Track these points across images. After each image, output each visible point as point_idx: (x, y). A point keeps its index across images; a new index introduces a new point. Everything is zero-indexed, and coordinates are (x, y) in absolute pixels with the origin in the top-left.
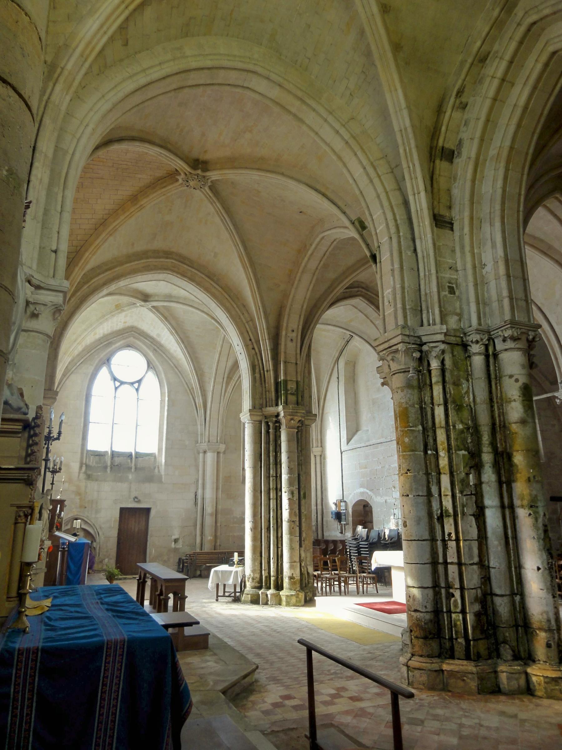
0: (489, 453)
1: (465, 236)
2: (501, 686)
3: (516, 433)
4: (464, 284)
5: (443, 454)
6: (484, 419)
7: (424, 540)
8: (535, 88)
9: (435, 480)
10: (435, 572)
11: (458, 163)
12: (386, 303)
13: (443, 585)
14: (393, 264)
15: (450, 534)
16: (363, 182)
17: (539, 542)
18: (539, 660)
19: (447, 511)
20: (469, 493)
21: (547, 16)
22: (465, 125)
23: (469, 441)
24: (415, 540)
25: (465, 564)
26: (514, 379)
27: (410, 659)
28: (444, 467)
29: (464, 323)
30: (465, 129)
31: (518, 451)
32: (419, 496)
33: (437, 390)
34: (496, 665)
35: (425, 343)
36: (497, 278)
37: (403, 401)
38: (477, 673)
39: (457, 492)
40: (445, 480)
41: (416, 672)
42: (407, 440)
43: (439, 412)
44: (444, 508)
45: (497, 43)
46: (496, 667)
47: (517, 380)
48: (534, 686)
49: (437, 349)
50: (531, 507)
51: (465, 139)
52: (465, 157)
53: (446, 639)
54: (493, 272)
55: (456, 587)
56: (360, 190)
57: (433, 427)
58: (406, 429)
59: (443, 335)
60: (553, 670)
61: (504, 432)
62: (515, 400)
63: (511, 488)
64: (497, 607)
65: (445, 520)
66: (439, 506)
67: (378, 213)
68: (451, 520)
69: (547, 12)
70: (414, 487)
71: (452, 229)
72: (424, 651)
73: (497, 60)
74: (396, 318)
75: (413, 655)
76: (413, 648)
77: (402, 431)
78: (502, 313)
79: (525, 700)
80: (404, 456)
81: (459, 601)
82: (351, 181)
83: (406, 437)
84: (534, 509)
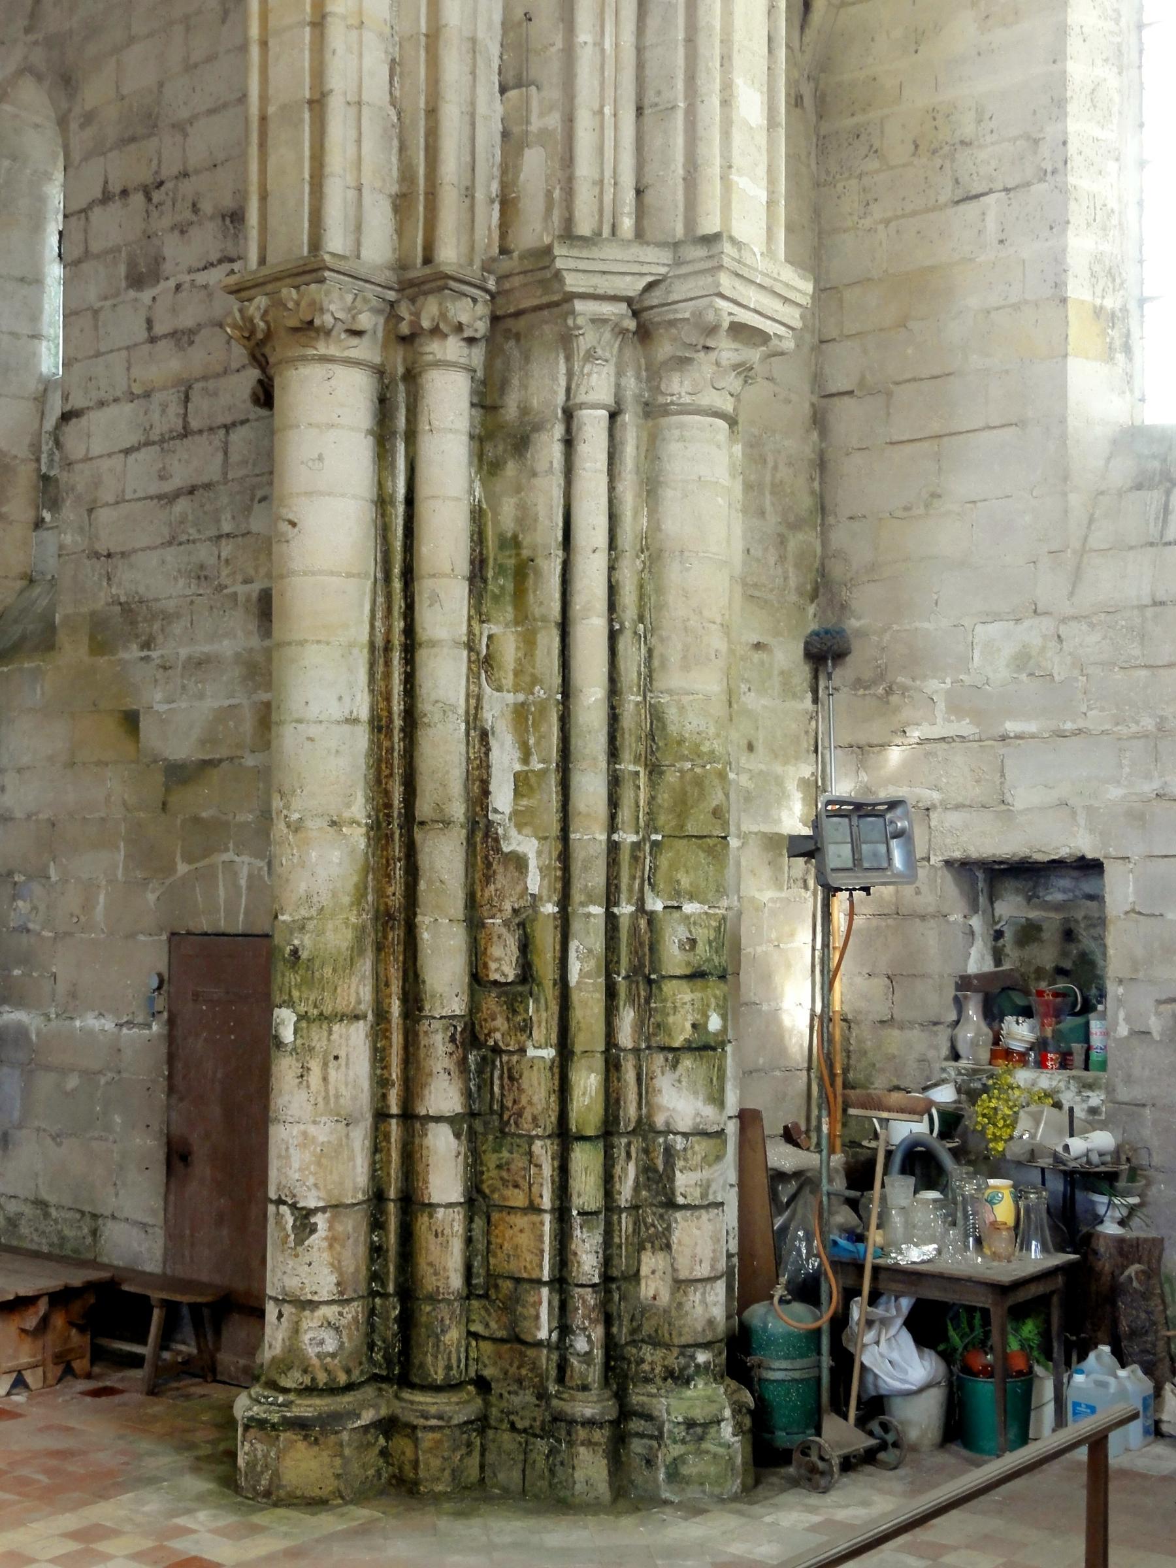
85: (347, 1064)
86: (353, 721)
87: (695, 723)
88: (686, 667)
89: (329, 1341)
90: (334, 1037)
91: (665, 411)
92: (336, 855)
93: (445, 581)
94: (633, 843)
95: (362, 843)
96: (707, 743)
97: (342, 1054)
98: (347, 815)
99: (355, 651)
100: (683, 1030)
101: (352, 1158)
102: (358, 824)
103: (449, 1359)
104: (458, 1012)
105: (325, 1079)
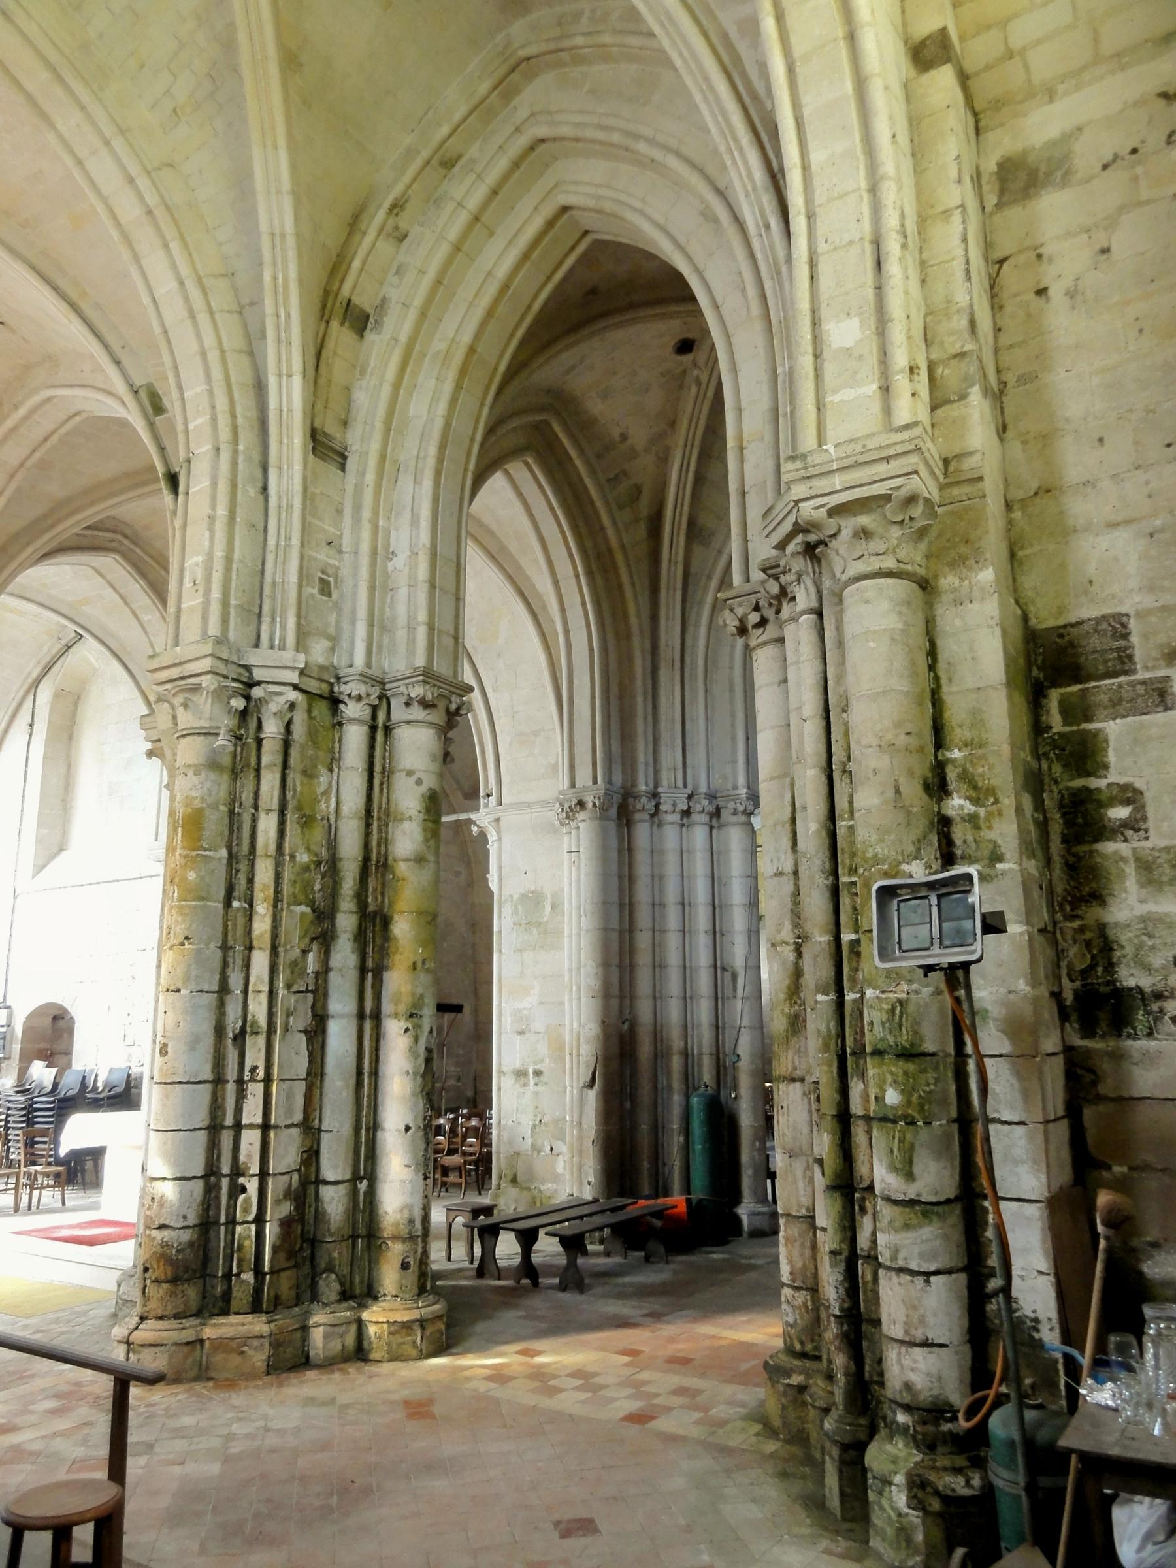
5: (262, 909)
7: (200, 1082)
8: (526, 256)
9: (239, 962)
10: (213, 1146)
11: (373, 342)
12: (188, 584)
13: (226, 1170)
15: (254, 1069)
16: (174, 311)
17: (415, 1079)
18: (385, 1295)
24: (180, 1082)
25: (276, 1127)
26: (415, 777)
27: (136, 1328)
29: (339, 656)
31: (402, 912)
32: (202, 991)
33: (270, 782)
34: (307, 1314)
35: (259, 683)
37: (194, 794)
38: (270, 1335)
39: (281, 985)
40: (260, 961)
41: (146, 1350)
42: (192, 876)
43: (267, 825)
44: (249, 1017)
46: (307, 1319)
47: (419, 782)
48: (371, 1343)
49: (281, 700)
50: (411, 1016)
51: (393, 301)
56: (163, 325)
59: (297, 673)
61: (383, 876)
64: (326, 1206)
65: (249, 1041)
66: (240, 1012)
68: (261, 1041)
69: (566, 131)
71: (343, 468)
72: (169, 1307)
74: (205, 618)
75: (143, 1319)
77: (186, 856)
78: (411, 652)
80: (180, 908)
82: (146, 300)
84: (415, 1020)
97: (785, 1106)
98: (778, 939)
99: (779, 828)
101: (795, 1182)
102: (787, 944)
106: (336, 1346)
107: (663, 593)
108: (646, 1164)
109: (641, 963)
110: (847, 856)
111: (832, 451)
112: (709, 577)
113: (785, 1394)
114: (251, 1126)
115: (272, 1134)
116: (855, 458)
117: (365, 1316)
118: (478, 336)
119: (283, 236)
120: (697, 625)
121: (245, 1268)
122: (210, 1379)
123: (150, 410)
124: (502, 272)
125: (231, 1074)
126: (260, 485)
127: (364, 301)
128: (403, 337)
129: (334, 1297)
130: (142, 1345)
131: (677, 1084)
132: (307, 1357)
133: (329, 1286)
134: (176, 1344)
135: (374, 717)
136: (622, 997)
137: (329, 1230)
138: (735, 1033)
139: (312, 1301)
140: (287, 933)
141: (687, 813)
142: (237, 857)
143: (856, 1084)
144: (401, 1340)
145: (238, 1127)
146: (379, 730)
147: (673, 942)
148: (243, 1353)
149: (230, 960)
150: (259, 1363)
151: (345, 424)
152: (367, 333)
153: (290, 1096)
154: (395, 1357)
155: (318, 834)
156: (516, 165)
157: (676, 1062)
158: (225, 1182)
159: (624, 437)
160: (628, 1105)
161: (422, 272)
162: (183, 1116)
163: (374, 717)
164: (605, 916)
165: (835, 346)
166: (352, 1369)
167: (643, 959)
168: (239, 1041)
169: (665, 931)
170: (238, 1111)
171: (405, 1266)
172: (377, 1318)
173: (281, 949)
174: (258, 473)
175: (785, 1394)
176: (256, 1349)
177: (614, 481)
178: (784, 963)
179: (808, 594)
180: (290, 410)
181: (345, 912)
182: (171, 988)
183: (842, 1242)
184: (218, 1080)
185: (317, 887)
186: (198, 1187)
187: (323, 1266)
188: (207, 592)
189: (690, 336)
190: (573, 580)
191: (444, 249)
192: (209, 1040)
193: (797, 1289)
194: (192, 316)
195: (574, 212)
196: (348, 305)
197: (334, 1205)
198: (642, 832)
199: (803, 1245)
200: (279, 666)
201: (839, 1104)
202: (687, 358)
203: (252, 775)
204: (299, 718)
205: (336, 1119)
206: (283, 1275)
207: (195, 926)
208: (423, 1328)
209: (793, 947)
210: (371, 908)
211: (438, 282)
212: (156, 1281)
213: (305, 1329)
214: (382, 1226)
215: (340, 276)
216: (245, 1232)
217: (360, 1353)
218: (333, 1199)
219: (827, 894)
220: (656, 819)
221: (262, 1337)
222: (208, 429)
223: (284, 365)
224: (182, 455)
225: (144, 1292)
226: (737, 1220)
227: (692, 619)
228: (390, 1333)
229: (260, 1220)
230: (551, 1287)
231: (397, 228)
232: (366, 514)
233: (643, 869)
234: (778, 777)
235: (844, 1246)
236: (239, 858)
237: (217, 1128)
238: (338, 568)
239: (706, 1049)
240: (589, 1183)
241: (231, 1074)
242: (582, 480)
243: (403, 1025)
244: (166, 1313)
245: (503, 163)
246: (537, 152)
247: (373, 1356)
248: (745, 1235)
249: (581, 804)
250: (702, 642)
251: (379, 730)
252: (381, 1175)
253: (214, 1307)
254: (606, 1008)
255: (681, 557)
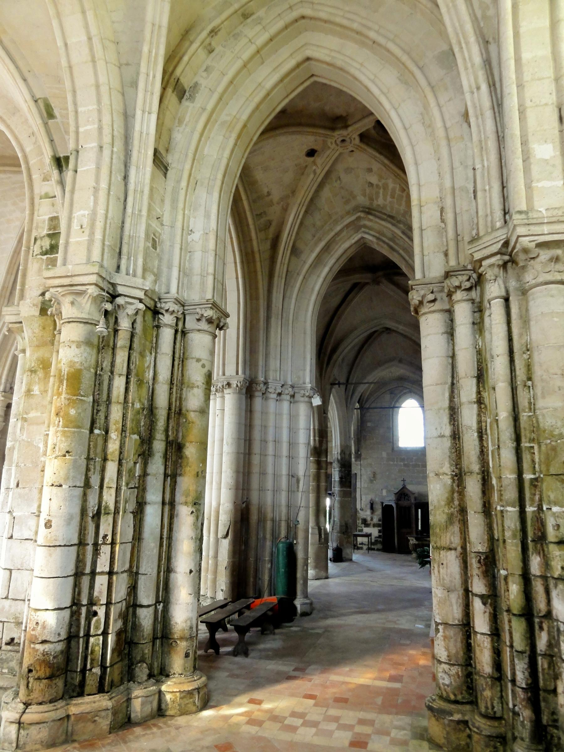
0: (162, 440)
1: (181, 191)
2: (133, 716)
3: (193, 423)
4: (168, 243)
5: (114, 435)
6: (162, 400)
7: (72, 545)
8: (281, 80)
9: (98, 468)
10: (77, 585)
11: (188, 107)
12: (75, 226)
13: (85, 602)
14: (97, 181)
15: (105, 536)
16: (79, 55)
17: (196, 542)
18: (174, 674)
19: (107, 507)
20: (133, 486)
21: (320, 19)
22: (206, 70)
23: (142, 424)
24: (60, 546)
25: (117, 573)
26: (201, 363)
27: (24, 712)
28: (113, 452)
29: (160, 286)
30: (204, 74)
31: (191, 442)
32: (75, 486)
33: (121, 357)
34: (128, 691)
35: (120, 295)
36: (205, 251)
37: (76, 360)
38: (112, 708)
39: (124, 484)
40: (112, 468)
41: (33, 727)
42: (73, 412)
43: (119, 383)
44: (104, 503)
45: (264, 9)
46: (129, 694)
47: (203, 366)
48: (167, 705)
49: (133, 307)
50: (195, 504)
51: (203, 86)
52: (199, 105)
53: (77, 672)
54: (201, 242)
55: (101, 603)
56: (69, 62)
57: (107, 400)
58: (75, 398)
59: (143, 293)
60: (189, 682)
61: (179, 419)
62: (198, 387)
63: (176, 482)
64: (141, 621)
65: (103, 519)
66: (97, 501)
67: (91, 108)
68: (110, 518)
69: (323, 15)
70: (72, 474)
71: (165, 175)
72: (47, 696)
73: (259, 27)
74: (89, 250)
75: (27, 705)
76: (29, 695)
77: (68, 399)
78: (203, 291)
79: (160, 725)
80: (64, 432)
81: (103, 621)
82: (60, 43)
83: (73, 407)
84: (197, 506)
85: (447, 568)
86: (441, 436)
87: (550, 422)
88: (543, 397)
89: (446, 679)
90: (441, 556)
91: (527, 291)
92: (438, 486)
93: (464, 380)
94: (531, 479)
95: (449, 482)
96: (557, 430)
97: (445, 563)
98: (441, 471)
99: (442, 411)
100: (557, 569)
101: (451, 605)
103: (487, 703)
104: (481, 551)
105: (439, 572)
106: (148, 709)
107: (276, 279)
108: (252, 579)
109: (254, 471)
110: (527, 432)
111: (544, 212)
112: (298, 274)
113: (449, 725)
114: (102, 573)
115: (115, 577)
116: (558, 218)
117: (164, 688)
118: (250, 117)
119: (160, 27)
120: (290, 298)
121: (95, 665)
122: (74, 741)
123: (45, 115)
124: (269, 85)
125: (90, 540)
126: (123, 175)
127: (186, 82)
128: (209, 107)
129: (145, 677)
130: (31, 724)
131: (268, 536)
132: (129, 718)
133: (142, 671)
134: (54, 721)
135: (177, 325)
136: (243, 489)
137: (143, 636)
138: (297, 509)
139: (129, 681)
140: (128, 451)
141: (280, 394)
142: (98, 402)
143: (536, 559)
144: (187, 702)
145: (93, 573)
146: (181, 333)
147: (270, 460)
148: (95, 721)
149: (92, 467)
150: (105, 727)
151: (167, 150)
152: (184, 101)
153: (124, 553)
154: (184, 712)
155: (144, 392)
156: (286, 27)
157: (269, 525)
158: (84, 610)
159: (269, 194)
160: (243, 547)
161: (223, 74)
162: (61, 567)
163: (177, 325)
164: (238, 446)
165: (538, 157)
166: (161, 722)
167: (255, 469)
168: (96, 518)
169: (266, 455)
170: (94, 564)
171: (187, 655)
172: (171, 689)
173: (124, 461)
174: (122, 167)
175: (449, 725)
176: (103, 718)
177: (259, 216)
178: (445, 485)
179: (500, 288)
180: (148, 134)
181: (159, 440)
182: (55, 484)
183: (526, 646)
184: (81, 544)
185: (142, 424)
186: (67, 614)
187: (138, 658)
188: (92, 233)
189: (315, 148)
190: (233, 265)
191: (239, 64)
192: (77, 518)
193: (453, 665)
194: (94, 61)
195: (312, 62)
196: (177, 81)
197: (146, 621)
198: (258, 402)
199: (456, 641)
200: (134, 285)
201: (522, 568)
202: (311, 159)
203: (110, 352)
204: (139, 319)
205: (149, 567)
206: (116, 666)
207: (73, 445)
208: (199, 693)
209: (450, 477)
210: (171, 438)
211: (231, 82)
212: (39, 679)
213: (129, 700)
214: (173, 631)
215: (174, 63)
216: (95, 642)
217: (160, 712)
218: (146, 616)
219: (514, 452)
220: (264, 396)
221: (108, 709)
222: (96, 133)
223: (148, 105)
224: (71, 146)
225: (28, 686)
226: (295, 608)
227: (288, 294)
228: (181, 698)
229: (105, 633)
230: (228, 654)
231: (210, 44)
232: (181, 205)
233: (257, 422)
234: (441, 384)
235: (528, 648)
236: (100, 404)
237: (81, 574)
238: (160, 234)
239: (283, 518)
240: (222, 590)
241: (90, 540)
242: (245, 212)
243: (190, 509)
244: (45, 700)
245: (280, 24)
246: (298, 23)
247: (169, 713)
248: (298, 615)
249: (229, 385)
250: (292, 307)
251: (181, 333)
252: (173, 599)
253: (73, 691)
254: (236, 496)
255: (287, 262)
